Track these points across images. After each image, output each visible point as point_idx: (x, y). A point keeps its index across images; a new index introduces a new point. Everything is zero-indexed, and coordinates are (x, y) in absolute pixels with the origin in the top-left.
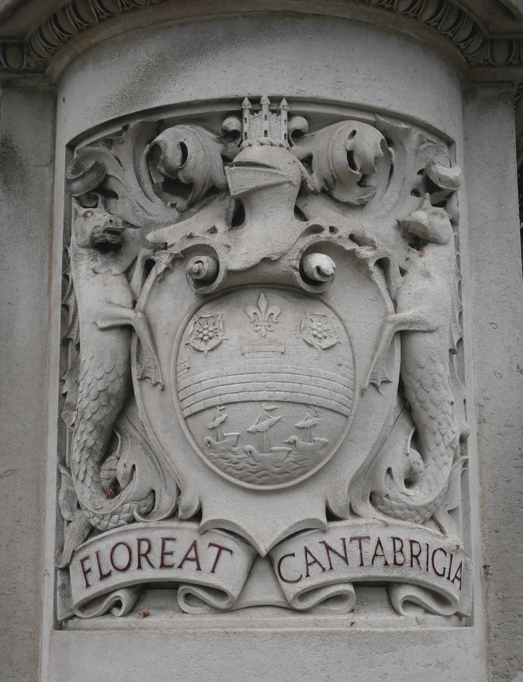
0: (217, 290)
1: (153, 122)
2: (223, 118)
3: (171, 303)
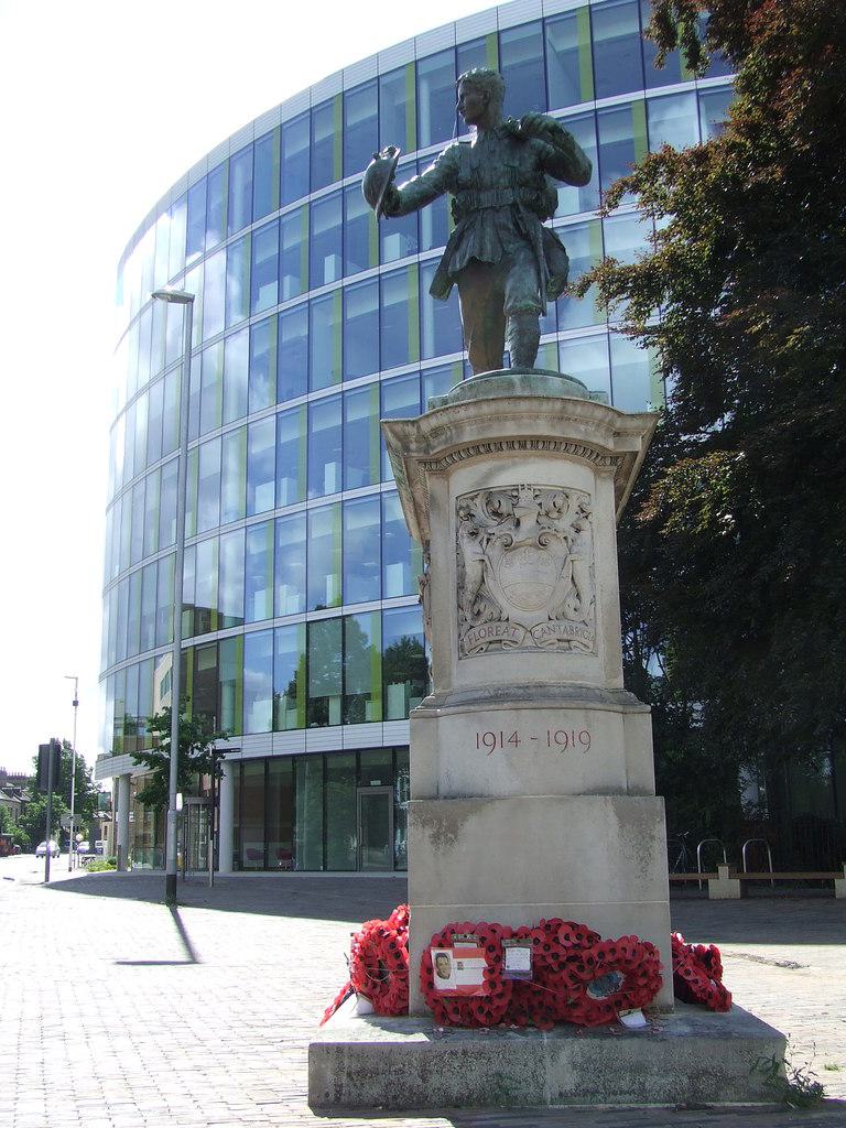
0: (508, 546)
1: (489, 496)
2: (513, 493)
3: (495, 551)
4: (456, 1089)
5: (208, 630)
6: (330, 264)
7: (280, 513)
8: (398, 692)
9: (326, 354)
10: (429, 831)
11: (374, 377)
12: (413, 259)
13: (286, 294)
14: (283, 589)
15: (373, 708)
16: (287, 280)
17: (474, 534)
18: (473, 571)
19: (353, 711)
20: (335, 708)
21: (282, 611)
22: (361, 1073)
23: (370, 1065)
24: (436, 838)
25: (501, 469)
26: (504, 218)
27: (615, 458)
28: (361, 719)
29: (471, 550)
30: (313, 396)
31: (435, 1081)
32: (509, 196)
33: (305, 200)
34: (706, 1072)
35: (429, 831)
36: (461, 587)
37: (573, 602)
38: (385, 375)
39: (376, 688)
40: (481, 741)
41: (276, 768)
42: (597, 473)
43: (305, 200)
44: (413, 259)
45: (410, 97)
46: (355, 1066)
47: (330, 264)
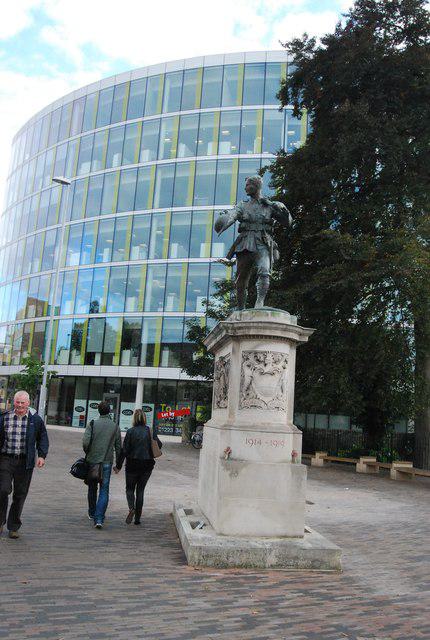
0: (262, 374)
1: (256, 353)
2: (265, 354)
4: (238, 562)
5: (43, 316)
6: (116, 158)
7: (81, 267)
8: (127, 353)
9: (110, 201)
10: (229, 472)
11: (131, 213)
12: (154, 163)
13: (94, 168)
14: (80, 302)
15: (116, 360)
16: (95, 162)
17: (249, 366)
18: (247, 380)
19: (107, 360)
20: (98, 359)
21: (77, 312)
22: (207, 556)
23: (210, 553)
24: (230, 475)
25: (258, 345)
26: (258, 235)
27: (297, 342)
28: (110, 364)
29: (248, 372)
30: (102, 217)
31: (231, 559)
32: (261, 228)
33: (107, 127)
34: (317, 560)
35: (229, 472)
36: (242, 384)
37: (281, 393)
38: (136, 213)
39: (117, 351)
40: (247, 441)
41: (66, 380)
42: (291, 346)
43: (107, 127)
44: (154, 163)
45: (161, 88)
46: (205, 554)
47: (116, 158)
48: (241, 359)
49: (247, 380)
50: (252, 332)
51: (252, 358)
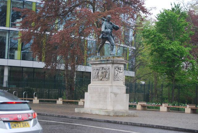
0: (120, 72)
3: (118, 72)
29: (116, 72)
48: (114, 69)
49: (116, 74)
50: (119, 62)
51: (117, 69)
